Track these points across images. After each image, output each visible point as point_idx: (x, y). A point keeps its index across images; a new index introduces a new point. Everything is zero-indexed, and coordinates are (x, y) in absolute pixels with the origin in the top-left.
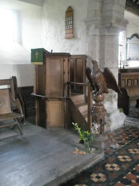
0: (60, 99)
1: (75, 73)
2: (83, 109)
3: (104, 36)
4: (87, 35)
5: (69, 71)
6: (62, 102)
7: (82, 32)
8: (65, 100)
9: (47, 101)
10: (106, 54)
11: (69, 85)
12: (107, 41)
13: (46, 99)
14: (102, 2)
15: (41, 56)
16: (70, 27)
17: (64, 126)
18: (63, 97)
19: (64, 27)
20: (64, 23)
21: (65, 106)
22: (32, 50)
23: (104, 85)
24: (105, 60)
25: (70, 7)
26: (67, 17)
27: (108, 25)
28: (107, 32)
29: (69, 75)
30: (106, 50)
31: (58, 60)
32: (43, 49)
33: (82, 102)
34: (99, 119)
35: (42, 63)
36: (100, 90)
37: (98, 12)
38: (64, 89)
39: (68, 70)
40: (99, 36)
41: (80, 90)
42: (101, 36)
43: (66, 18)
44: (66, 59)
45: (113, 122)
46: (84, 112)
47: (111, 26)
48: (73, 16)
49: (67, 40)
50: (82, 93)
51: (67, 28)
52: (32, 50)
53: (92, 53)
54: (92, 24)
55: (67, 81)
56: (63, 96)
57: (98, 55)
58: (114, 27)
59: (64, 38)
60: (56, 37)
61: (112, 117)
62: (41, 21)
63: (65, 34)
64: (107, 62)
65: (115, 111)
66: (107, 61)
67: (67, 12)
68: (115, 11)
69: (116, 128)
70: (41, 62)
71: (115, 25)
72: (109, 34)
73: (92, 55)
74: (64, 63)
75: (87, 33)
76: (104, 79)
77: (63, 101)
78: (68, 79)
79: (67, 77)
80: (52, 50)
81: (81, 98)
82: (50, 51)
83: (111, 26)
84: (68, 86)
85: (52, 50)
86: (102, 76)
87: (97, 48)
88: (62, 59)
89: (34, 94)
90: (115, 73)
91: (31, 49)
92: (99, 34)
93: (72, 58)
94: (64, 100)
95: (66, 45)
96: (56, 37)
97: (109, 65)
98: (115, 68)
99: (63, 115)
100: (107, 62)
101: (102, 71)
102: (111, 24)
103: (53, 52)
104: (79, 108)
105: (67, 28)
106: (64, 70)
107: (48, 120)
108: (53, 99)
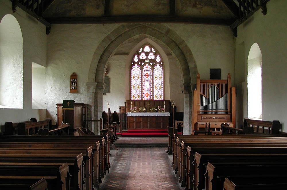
4: (88, 92)
7: (84, 90)
16: (74, 83)
20: (68, 82)
43: (71, 79)
60: (61, 90)
62: (45, 78)
67: (71, 76)
70: (91, 124)
75: (88, 91)
96: (61, 90)
104: (18, 7)
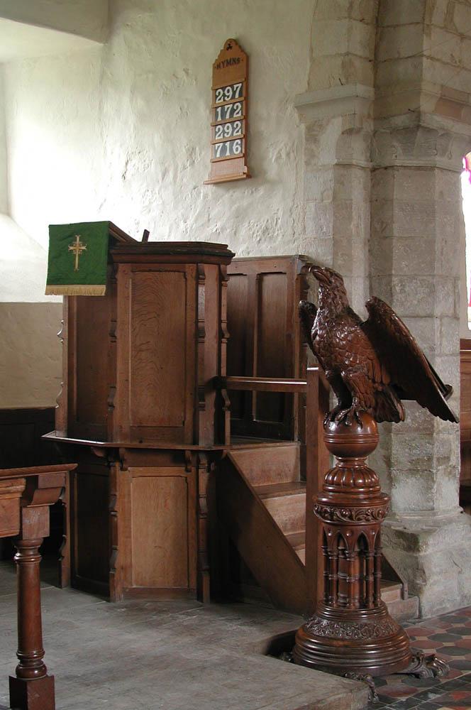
0: (178, 458)
1: (255, 353)
2: (287, 510)
3: (386, 168)
4: (307, 163)
5: (224, 326)
6: (187, 471)
7: (288, 154)
8: (204, 461)
9: (117, 465)
10: (398, 249)
11: (224, 392)
12: (402, 191)
13: (112, 454)
14: (377, 21)
15: (88, 252)
16: (233, 111)
17: (194, 585)
18: (194, 448)
19: (207, 133)
21: (203, 490)
22: (55, 231)
23: (378, 379)
24: (395, 280)
25: (231, 45)
26: (219, 84)
27: (401, 121)
28: (400, 151)
29: (224, 346)
30: (396, 233)
31: (173, 276)
32: (110, 225)
33: (289, 480)
34: (352, 532)
35: (100, 290)
37: (358, 63)
38: (197, 408)
39: (220, 321)
41: (276, 419)
42: (374, 170)
44: (210, 272)
45: (435, 578)
46: (294, 526)
47: (418, 126)
48: (246, 81)
49: (220, 191)
50: (288, 438)
51: (219, 119)
52: (55, 231)
53: (339, 243)
54: (334, 117)
55: (214, 374)
56: (195, 442)
57: (362, 256)
58: (429, 130)
59: (206, 178)
61: (433, 553)
62: (101, 108)
63: (209, 164)
64: (402, 291)
65: (445, 524)
66: (403, 286)
67: (219, 66)
68: (432, 58)
69: (449, 608)
71: (435, 120)
72: (408, 163)
73: (335, 254)
74: (201, 290)
75: (311, 156)
76: (370, 352)
77: (194, 469)
79: (215, 352)
80: (146, 233)
81: (284, 454)
82: (138, 237)
83: (418, 126)
84: (219, 396)
85: (146, 233)
87: (359, 224)
88: (190, 269)
89: (57, 435)
90: (445, 343)
91: (51, 227)
92: (363, 163)
93: (242, 274)
94: (198, 461)
95: (212, 214)
96: (171, 174)
97: (415, 302)
98: (441, 318)
99: (192, 533)
100: (402, 291)
102: (417, 113)
103: (150, 239)
105: (219, 119)
106: (197, 321)
107: (120, 559)
108: (145, 454)
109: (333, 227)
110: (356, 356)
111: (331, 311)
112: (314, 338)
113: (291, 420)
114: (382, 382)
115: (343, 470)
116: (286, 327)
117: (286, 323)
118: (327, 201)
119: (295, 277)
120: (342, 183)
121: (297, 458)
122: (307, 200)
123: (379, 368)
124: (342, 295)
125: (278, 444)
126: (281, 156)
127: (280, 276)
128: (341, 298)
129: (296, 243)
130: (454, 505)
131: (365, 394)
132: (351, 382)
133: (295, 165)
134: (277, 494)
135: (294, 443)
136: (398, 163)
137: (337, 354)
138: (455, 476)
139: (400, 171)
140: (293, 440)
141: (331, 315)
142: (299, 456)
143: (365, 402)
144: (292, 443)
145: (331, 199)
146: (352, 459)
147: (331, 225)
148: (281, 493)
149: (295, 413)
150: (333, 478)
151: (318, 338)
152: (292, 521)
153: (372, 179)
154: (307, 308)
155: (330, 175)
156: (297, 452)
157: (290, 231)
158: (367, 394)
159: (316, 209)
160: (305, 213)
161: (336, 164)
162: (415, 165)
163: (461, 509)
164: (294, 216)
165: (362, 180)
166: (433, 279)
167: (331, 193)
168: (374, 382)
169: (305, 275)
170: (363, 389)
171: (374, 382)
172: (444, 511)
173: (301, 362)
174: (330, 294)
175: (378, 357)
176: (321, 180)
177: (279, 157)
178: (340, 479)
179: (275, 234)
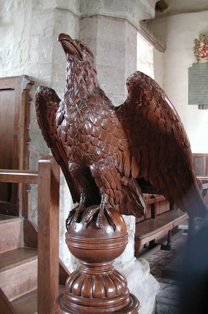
4: (34, 9)
23: (127, 172)
28: (103, 5)
33: (16, 247)
36: (105, 199)
40: (75, 16)
42: (82, 18)
50: (14, 214)
73: (53, 74)
76: (122, 142)
78: (157, 232)
86: (116, 121)
101: (119, 96)
109: (53, 54)
110: (108, 146)
111: (81, 90)
112: (60, 123)
113: (17, 200)
114: (131, 176)
115: (92, 278)
116: (13, 129)
117: (13, 127)
118: (49, 35)
119: (22, 91)
120: (60, 23)
121: (21, 229)
122: (32, 36)
123: (129, 161)
124: (94, 73)
125: (7, 221)
126: (13, 5)
127: (9, 92)
128: (92, 76)
129: (22, 67)
130: (131, 257)
131: (115, 191)
132: (103, 177)
133: (24, 11)
134: (7, 267)
135: (19, 219)
136: (101, 12)
137: (88, 143)
138: (132, 237)
139: (102, 19)
140: (18, 216)
141: (82, 95)
142: (23, 228)
143: (115, 200)
144: (17, 219)
145: (52, 34)
146: (99, 264)
147: (51, 53)
148: (11, 266)
149: (19, 196)
150: (80, 287)
151: (64, 123)
152: (19, 287)
153: (80, 25)
154: (46, 93)
155: (51, 16)
156: (21, 225)
157: (18, 59)
158: (117, 190)
159: (39, 41)
160: (30, 45)
161: (57, 8)
162: (112, 16)
163: (135, 259)
164: (21, 48)
165: (73, 23)
166: (123, 97)
167: (51, 29)
168: (122, 174)
169: (29, 90)
170: (114, 185)
171: (122, 174)
172: (127, 262)
173: (24, 157)
174: (80, 70)
175: (130, 149)
176: (44, 20)
177: (12, 6)
178: (87, 288)
179: (7, 62)
